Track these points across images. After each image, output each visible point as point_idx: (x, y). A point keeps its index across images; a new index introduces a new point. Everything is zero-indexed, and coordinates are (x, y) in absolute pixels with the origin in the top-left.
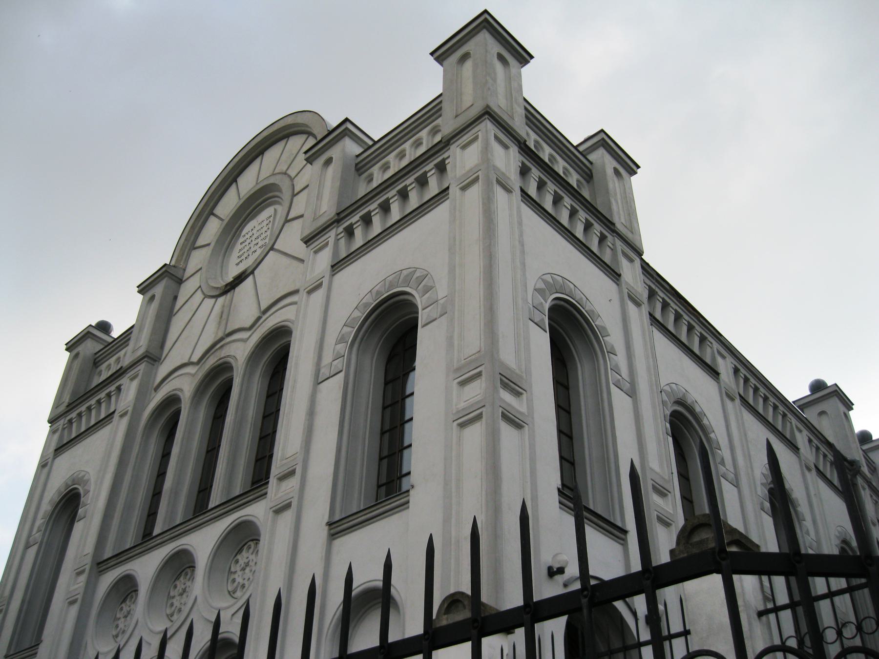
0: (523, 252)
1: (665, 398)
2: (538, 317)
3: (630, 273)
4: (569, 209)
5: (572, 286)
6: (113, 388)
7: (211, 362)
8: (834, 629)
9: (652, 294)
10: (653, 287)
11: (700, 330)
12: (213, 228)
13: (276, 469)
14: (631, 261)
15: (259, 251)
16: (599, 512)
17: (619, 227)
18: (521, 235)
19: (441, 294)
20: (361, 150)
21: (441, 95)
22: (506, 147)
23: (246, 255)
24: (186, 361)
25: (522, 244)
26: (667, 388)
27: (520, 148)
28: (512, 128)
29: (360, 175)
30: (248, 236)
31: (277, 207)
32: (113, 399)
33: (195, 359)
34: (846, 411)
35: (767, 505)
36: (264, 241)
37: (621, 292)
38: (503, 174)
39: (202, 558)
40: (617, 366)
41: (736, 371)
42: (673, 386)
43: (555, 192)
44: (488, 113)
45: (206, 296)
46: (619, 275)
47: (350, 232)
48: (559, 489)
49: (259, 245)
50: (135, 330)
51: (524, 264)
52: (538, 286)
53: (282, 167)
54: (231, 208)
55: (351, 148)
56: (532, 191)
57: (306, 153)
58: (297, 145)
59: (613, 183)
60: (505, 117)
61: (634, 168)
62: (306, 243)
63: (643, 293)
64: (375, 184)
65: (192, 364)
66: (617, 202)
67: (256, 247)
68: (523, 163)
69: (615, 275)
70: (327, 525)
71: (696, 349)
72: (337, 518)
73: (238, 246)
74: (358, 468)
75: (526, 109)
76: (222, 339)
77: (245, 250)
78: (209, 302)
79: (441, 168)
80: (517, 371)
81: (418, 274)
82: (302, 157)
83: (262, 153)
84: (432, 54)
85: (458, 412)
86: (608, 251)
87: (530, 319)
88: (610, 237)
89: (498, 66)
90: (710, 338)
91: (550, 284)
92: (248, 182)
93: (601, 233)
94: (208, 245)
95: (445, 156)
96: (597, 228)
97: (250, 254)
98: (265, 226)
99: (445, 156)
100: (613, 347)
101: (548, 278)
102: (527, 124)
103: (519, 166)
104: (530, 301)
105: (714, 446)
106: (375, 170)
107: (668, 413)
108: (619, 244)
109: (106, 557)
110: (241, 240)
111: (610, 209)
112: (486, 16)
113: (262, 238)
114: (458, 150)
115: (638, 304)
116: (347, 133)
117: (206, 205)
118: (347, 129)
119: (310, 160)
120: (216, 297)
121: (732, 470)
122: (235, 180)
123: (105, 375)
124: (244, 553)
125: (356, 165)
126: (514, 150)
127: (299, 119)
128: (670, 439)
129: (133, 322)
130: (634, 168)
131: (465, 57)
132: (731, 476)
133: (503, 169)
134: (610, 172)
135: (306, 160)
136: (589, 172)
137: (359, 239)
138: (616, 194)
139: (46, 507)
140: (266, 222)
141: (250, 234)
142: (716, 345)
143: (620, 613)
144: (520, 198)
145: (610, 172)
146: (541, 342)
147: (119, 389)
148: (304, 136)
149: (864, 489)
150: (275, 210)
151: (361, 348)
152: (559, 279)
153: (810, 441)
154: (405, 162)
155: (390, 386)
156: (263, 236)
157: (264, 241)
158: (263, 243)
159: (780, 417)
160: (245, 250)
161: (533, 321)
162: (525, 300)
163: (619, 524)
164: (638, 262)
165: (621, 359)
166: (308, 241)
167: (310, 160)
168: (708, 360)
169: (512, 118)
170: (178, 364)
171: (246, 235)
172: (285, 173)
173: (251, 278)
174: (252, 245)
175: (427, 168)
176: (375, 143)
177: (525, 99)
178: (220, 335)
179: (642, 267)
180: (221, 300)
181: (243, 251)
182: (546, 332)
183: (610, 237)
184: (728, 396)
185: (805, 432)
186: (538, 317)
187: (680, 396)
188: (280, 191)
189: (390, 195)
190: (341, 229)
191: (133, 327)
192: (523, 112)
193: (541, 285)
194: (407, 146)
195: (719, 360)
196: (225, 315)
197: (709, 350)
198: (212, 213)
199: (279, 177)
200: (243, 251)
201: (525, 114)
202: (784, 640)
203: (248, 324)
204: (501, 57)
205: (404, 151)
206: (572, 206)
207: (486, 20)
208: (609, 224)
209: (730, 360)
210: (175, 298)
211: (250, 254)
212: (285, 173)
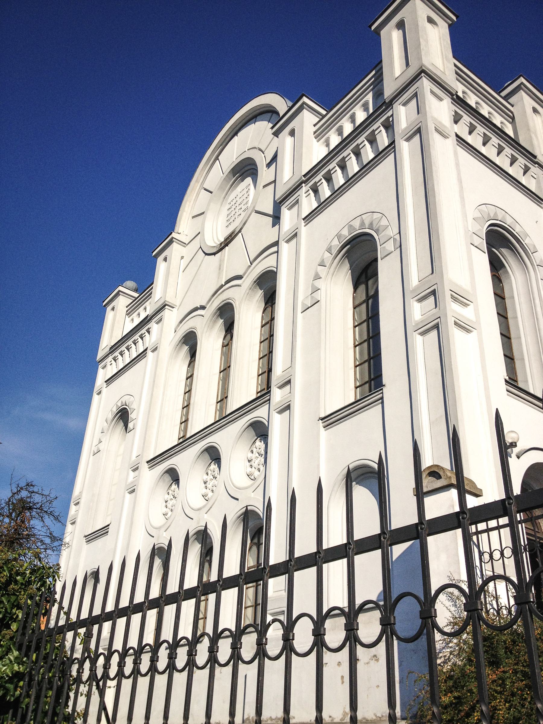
4: (497, 148)
6: (144, 331)
8: (500, 551)
15: (243, 214)
23: (233, 218)
27: (453, 99)
28: (445, 82)
30: (233, 203)
36: (246, 206)
44: (423, 71)
48: (506, 381)
49: (243, 209)
52: (475, 216)
54: (182, 222)
67: (241, 211)
68: (456, 112)
70: (384, 385)
77: (232, 214)
79: (389, 126)
87: (471, 244)
97: (237, 217)
98: (245, 194)
99: (390, 114)
102: (457, 79)
103: (453, 115)
111: (532, 145)
113: (244, 203)
118: (304, 103)
126: (447, 101)
134: (530, 111)
136: (512, 115)
141: (234, 201)
143: (475, 507)
144: (456, 142)
151: (332, 282)
155: (357, 309)
156: (245, 202)
157: (246, 206)
158: (245, 207)
160: (232, 214)
161: (474, 245)
171: (231, 202)
174: (237, 210)
181: (230, 216)
182: (485, 253)
200: (230, 216)
201: (455, 70)
202: (492, 552)
206: (499, 145)
211: (237, 217)
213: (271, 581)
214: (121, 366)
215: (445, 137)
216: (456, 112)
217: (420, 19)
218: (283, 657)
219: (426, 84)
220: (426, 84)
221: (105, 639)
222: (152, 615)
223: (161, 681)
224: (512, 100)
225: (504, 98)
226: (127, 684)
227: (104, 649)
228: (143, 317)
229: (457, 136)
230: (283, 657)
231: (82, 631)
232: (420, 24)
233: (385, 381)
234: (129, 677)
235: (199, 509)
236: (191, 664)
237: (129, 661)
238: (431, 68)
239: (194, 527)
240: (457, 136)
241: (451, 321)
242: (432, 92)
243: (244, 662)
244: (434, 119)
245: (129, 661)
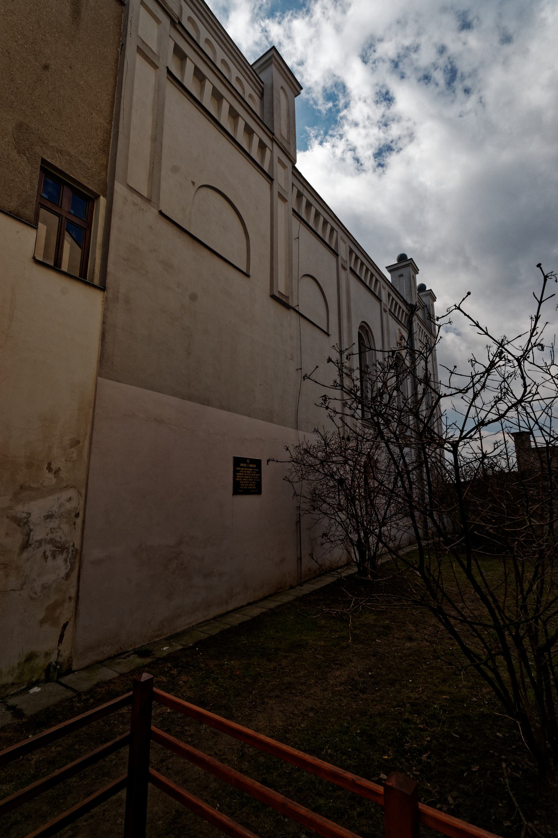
14: (284, 166)
22: (158, 21)
34: (414, 274)
108: (277, 152)
115: (284, 200)
126: (166, 21)
153: (389, 295)
168: (333, 246)
185: (388, 289)
215: (155, 67)
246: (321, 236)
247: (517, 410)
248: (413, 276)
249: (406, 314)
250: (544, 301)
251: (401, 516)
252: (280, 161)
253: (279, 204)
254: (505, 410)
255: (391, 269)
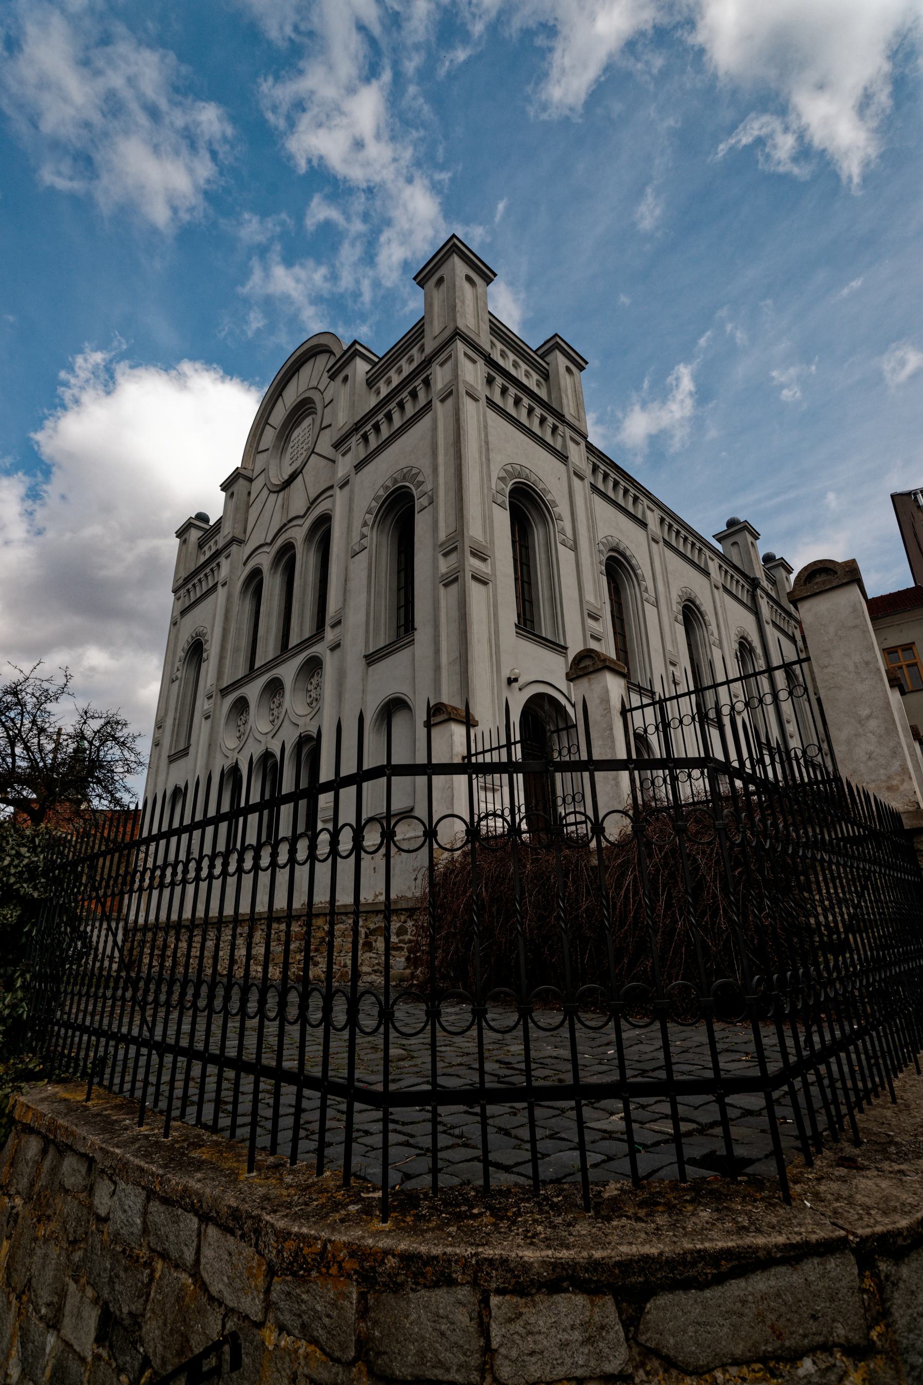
0: (488, 450)
1: (602, 547)
2: (500, 499)
3: (577, 454)
5: (528, 471)
7: (279, 542)
9: (595, 469)
10: (595, 461)
11: (633, 491)
12: (269, 436)
13: (329, 621)
14: (578, 444)
15: (305, 454)
16: (549, 638)
17: (568, 417)
18: (486, 436)
19: (430, 487)
20: (369, 367)
21: (423, 318)
22: (474, 362)
24: (262, 542)
25: (487, 443)
26: (605, 540)
27: (486, 360)
29: (371, 388)
31: (314, 416)
32: (216, 573)
33: (268, 541)
34: (753, 540)
35: (680, 617)
37: (568, 470)
38: (471, 386)
39: (288, 683)
40: (563, 529)
41: (662, 520)
42: (610, 538)
43: (516, 395)
44: (458, 334)
45: (271, 492)
46: (567, 458)
47: (365, 438)
50: (426, 320)
51: (488, 460)
52: (500, 475)
53: (314, 383)
55: (361, 367)
56: (497, 398)
57: (328, 371)
58: (322, 363)
59: (566, 381)
60: (472, 336)
61: (583, 364)
62: (335, 448)
63: (586, 469)
64: (383, 395)
65: (267, 544)
66: (567, 396)
67: (303, 451)
68: (489, 374)
69: (563, 457)
71: (631, 509)
72: (371, 651)
73: (290, 450)
74: (383, 614)
75: (490, 321)
76: (285, 525)
78: (273, 497)
79: (427, 383)
80: (484, 543)
81: (413, 472)
82: (326, 375)
83: (298, 370)
84: (415, 279)
85: (442, 576)
86: (559, 438)
88: (561, 427)
89: (467, 286)
90: (641, 497)
91: (510, 472)
92: (291, 396)
93: (554, 424)
94: (268, 450)
95: (428, 372)
96: (551, 420)
99: (428, 372)
100: (560, 515)
101: (509, 468)
104: (493, 486)
105: (640, 578)
106: (382, 385)
107: (604, 558)
108: (568, 432)
109: (225, 685)
110: (291, 444)
112: (455, 240)
114: (438, 367)
115: (581, 478)
116: (357, 353)
117: (262, 416)
118: (356, 349)
119: (332, 378)
120: (278, 492)
121: (654, 595)
122: (280, 395)
123: (208, 555)
124: (315, 677)
125: (367, 380)
126: (481, 362)
127: (323, 340)
128: (604, 579)
129: (221, 514)
130: (583, 364)
131: (441, 281)
132: (653, 599)
133: (472, 383)
134: (562, 370)
135: (329, 377)
137: (373, 442)
138: (566, 390)
139: (181, 654)
140: (307, 430)
142: (646, 502)
144: (486, 404)
145: (562, 370)
146: (502, 519)
147: (218, 565)
148: (328, 355)
149: (762, 598)
150: (313, 419)
152: (518, 467)
153: (720, 567)
154: (415, 364)
159: (697, 551)
162: (490, 488)
163: (562, 643)
164: (583, 444)
165: (567, 525)
166: (336, 446)
167: (332, 378)
168: (640, 516)
169: (478, 335)
170: (258, 545)
172: (316, 388)
173: (300, 477)
175: (416, 384)
176: (381, 359)
177: (490, 313)
178: (285, 521)
179: (587, 447)
180: (281, 494)
183: (561, 427)
184: (654, 540)
185: (717, 561)
186: (500, 499)
187: (614, 544)
188: (314, 403)
189: (391, 407)
190: (359, 436)
191: (221, 518)
192: (488, 323)
193: (503, 474)
194: (403, 362)
195: (648, 513)
196: (285, 507)
197: (640, 507)
198: (267, 423)
199: (312, 391)
203: (302, 514)
204: (469, 279)
205: (412, 356)
207: (455, 245)
208: (560, 417)
209: (658, 513)
210: (249, 493)
212: (316, 388)
213: (282, 807)
214: (193, 600)
215: (476, 400)
216: (489, 374)
217: (458, 280)
218: (330, 859)
219: (460, 347)
220: (460, 347)
221: (324, 809)
222: (163, 843)
223: (232, 881)
224: (547, 359)
225: (539, 356)
226: (204, 885)
227: (324, 821)
228: (214, 550)
229: (487, 398)
230: (330, 859)
231: (126, 852)
232: (457, 283)
233: (416, 625)
234: (266, 870)
235: (267, 733)
236: (256, 867)
237: (219, 862)
238: (464, 330)
239: (228, 763)
240: (487, 398)
241: (468, 576)
242: (466, 354)
243: (342, 857)
244: (465, 382)
245: (219, 862)
246: (623, 505)
247: (290, 1106)
248: (752, 543)
249: (748, 591)
250: (707, 1135)
251: (42, 1181)
252: (572, 439)
253: (576, 481)
254: (625, 1051)
255: (720, 538)
